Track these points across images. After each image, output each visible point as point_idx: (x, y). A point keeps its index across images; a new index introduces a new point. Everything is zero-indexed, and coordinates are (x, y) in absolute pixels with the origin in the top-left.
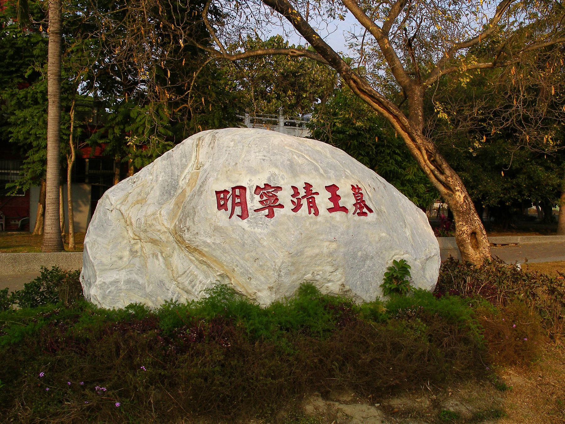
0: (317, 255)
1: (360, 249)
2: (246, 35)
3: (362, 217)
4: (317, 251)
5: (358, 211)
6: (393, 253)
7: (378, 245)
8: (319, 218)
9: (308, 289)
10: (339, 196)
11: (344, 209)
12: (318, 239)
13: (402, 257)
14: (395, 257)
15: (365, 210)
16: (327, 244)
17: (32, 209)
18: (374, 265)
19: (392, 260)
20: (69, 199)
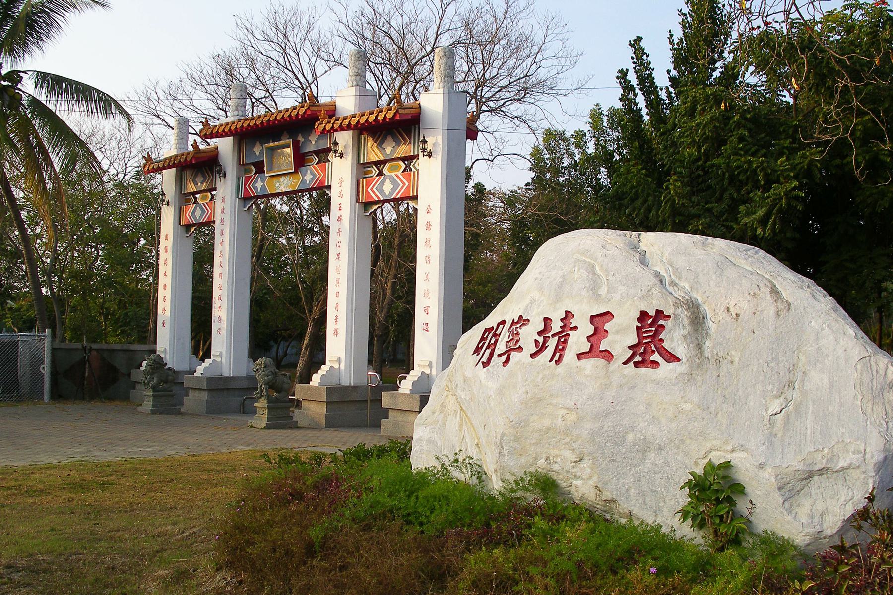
1: (632, 429)
2: (351, 48)
3: (643, 371)
4: (547, 422)
5: (638, 358)
6: (709, 445)
7: (673, 426)
8: (561, 369)
9: (546, 484)
10: (606, 331)
11: (608, 355)
13: (729, 457)
14: (714, 453)
15: (656, 357)
16: (563, 412)
17: (172, 344)
19: (707, 460)
20: (306, 342)
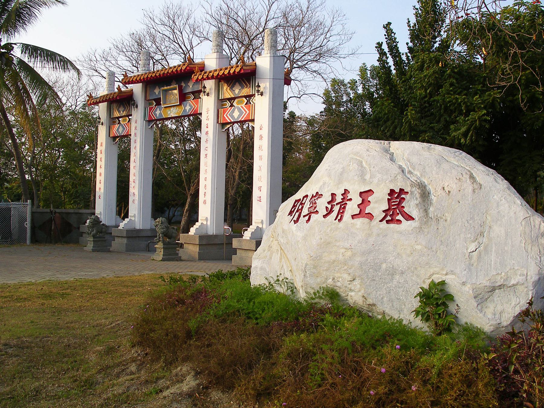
0: (334, 261)
3: (392, 225)
4: (333, 257)
5: (389, 218)
6: (432, 271)
8: (341, 224)
9: (333, 295)
10: (369, 201)
11: (370, 216)
12: (335, 246)
13: (444, 278)
14: (435, 276)
15: (399, 217)
16: (343, 250)
17: (105, 209)
18: (406, 281)
19: (431, 280)
20: (186, 208)
